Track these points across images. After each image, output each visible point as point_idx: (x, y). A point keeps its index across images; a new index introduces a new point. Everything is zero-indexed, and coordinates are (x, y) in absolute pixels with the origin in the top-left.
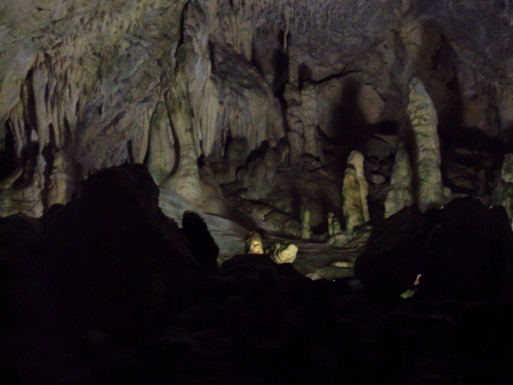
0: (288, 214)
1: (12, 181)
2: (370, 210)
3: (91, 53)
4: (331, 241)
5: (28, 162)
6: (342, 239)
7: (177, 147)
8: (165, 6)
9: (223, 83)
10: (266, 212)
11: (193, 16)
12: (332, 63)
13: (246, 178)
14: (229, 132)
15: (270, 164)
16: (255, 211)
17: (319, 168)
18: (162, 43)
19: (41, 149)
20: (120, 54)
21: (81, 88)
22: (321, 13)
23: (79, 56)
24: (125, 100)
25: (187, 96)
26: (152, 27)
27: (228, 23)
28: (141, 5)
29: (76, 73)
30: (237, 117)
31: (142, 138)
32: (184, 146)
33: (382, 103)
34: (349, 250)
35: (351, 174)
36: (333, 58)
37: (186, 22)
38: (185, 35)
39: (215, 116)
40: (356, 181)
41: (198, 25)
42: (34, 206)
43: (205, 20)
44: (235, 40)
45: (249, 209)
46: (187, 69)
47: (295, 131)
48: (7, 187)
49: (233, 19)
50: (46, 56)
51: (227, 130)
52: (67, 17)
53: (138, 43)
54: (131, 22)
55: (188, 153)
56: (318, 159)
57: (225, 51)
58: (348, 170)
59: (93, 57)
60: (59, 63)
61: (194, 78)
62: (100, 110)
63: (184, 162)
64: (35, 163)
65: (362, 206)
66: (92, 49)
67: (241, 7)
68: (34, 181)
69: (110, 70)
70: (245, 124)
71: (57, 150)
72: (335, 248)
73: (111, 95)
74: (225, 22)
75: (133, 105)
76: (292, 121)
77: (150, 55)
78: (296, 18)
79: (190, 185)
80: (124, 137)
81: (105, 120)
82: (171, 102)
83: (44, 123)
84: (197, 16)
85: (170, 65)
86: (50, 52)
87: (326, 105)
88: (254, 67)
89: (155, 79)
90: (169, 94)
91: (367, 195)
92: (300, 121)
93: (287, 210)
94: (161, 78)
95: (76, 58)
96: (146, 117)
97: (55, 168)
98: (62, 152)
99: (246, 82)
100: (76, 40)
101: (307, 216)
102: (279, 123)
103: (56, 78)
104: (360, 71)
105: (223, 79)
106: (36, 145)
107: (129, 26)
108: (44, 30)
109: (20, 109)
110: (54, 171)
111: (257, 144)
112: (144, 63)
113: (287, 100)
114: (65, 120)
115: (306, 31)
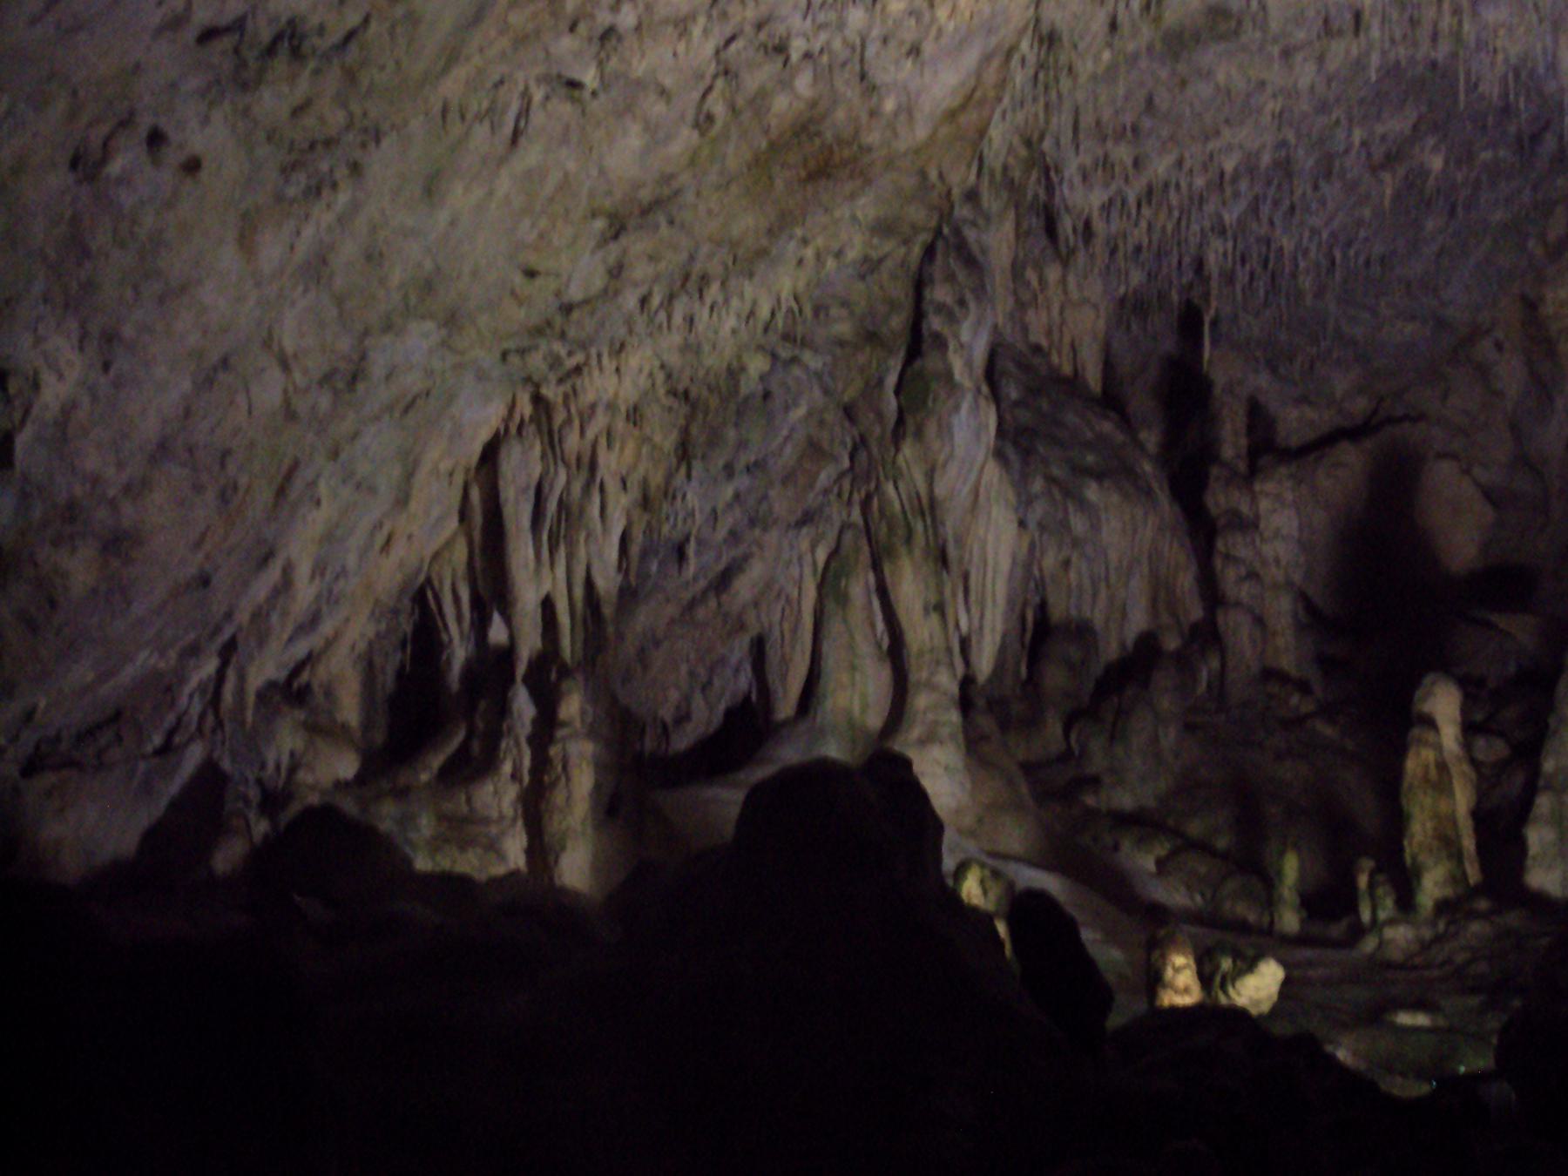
0: (1224, 856)
1: (437, 761)
2: (1480, 848)
3: (661, 391)
4: (1369, 944)
5: (482, 705)
6: (1400, 936)
7: (896, 652)
8: (875, 255)
9: (1025, 462)
10: (1162, 849)
11: (951, 278)
12: (1339, 394)
13: (1096, 746)
14: (1043, 607)
15: (1166, 703)
16: (1126, 845)
17: (1308, 716)
18: (861, 359)
19: (521, 669)
20: (745, 389)
21: (635, 493)
22: (1312, 254)
23: (631, 403)
24: (753, 522)
25: (930, 508)
26: (835, 311)
27: (1035, 283)
28: (809, 253)
29: (622, 449)
30: (1066, 564)
31: (794, 630)
32: (921, 653)
33: (1488, 514)
34: (1427, 973)
35: (1426, 744)
36: (1341, 384)
37: (927, 294)
38: (925, 332)
39: (1005, 565)
40: (1442, 767)
41: (962, 303)
42: (503, 833)
43: (983, 286)
44: (1056, 336)
45: (1108, 840)
46: (931, 429)
47: (1238, 604)
48: (424, 777)
49: (1053, 273)
50: (537, 399)
51: (1037, 599)
52: (605, 291)
53: (794, 360)
54: (779, 301)
55: (932, 674)
56: (1304, 687)
57: (1025, 368)
58: (1416, 732)
59: (668, 401)
60: (576, 423)
61: (951, 456)
62: (680, 553)
63: (921, 701)
64: (503, 709)
65: (1459, 837)
66: (669, 376)
67: (1081, 245)
68: (502, 762)
69: (715, 439)
70: (1087, 583)
71: (565, 672)
72: (1381, 965)
73: (714, 511)
74: (1028, 284)
75: (773, 537)
76: (1229, 577)
77: (826, 392)
78: (1239, 273)
79: (940, 771)
80: (741, 626)
81: (695, 579)
82: (884, 529)
83: (528, 597)
84: (961, 276)
85: (880, 416)
86: (551, 392)
87: (1320, 518)
88: (1112, 414)
89: (836, 459)
90: (875, 503)
91: (1472, 804)
92: (1253, 575)
93: (1222, 843)
94: (852, 457)
95: (623, 409)
96: (808, 571)
97: (563, 724)
98: (580, 677)
99: (1090, 458)
100: (623, 355)
101: (1291, 868)
102: (1186, 581)
103: (567, 465)
104: (1422, 417)
105: (1027, 453)
106: (507, 655)
107: (773, 314)
108: (539, 331)
109: (460, 553)
110: (560, 733)
111: (1123, 645)
112: (809, 414)
113: (1214, 511)
114: (589, 584)
115: (1266, 304)
